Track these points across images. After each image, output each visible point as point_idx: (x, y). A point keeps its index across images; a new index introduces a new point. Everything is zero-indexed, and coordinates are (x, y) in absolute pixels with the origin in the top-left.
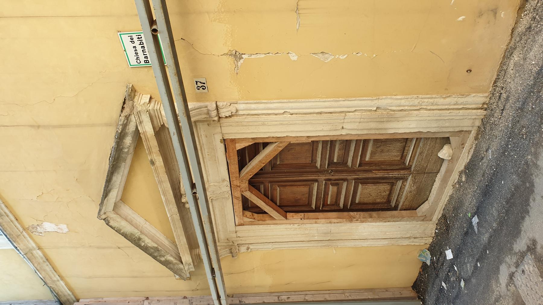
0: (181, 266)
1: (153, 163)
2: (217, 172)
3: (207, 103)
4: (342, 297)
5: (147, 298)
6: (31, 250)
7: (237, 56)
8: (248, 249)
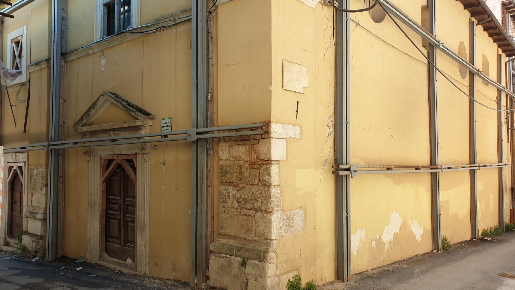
0: (80, 126)
1: (125, 122)
2: (124, 150)
3: (149, 149)
4: (60, 214)
5: (65, 101)
6: (93, 49)
7: (164, 164)
8: (88, 161)
